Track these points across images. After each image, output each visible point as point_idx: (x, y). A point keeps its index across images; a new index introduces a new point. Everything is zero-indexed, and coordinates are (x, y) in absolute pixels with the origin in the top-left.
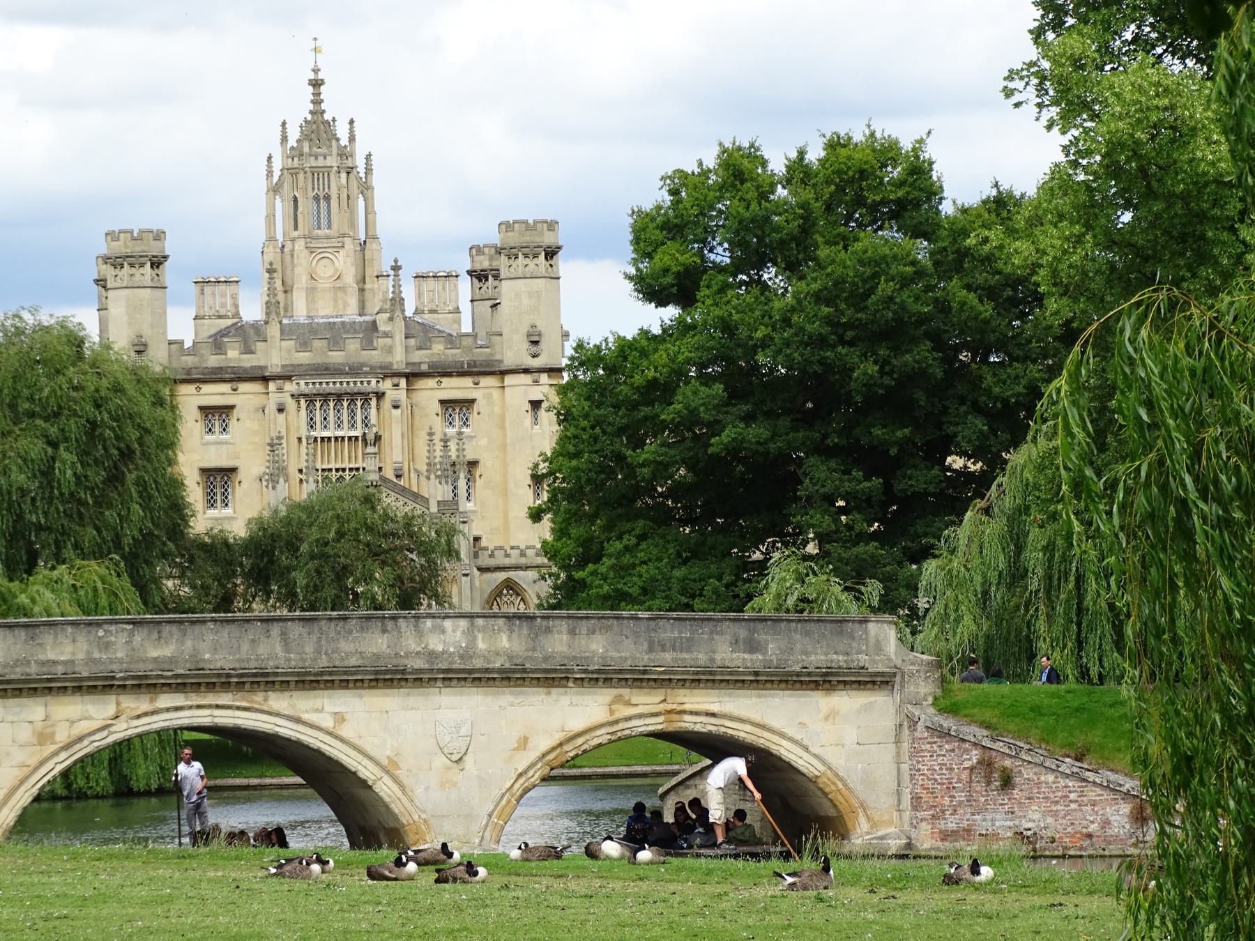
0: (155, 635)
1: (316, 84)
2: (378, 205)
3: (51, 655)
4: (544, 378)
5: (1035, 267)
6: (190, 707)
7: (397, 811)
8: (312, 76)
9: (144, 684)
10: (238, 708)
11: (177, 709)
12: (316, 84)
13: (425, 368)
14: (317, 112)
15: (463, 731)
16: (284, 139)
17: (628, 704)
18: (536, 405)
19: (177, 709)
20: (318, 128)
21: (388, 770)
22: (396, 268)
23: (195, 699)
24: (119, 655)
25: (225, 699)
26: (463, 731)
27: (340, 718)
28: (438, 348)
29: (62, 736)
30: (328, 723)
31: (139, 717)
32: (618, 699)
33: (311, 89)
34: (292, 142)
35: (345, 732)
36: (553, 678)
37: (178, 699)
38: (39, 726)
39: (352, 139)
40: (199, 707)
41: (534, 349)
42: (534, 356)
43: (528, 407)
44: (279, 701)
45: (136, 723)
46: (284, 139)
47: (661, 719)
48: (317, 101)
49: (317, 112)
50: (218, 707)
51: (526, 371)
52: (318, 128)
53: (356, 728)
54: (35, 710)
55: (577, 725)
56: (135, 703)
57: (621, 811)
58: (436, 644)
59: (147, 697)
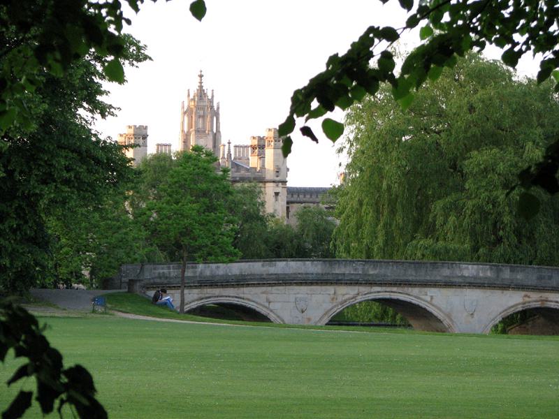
0: (372, 266)
1: (201, 76)
2: (221, 121)
3: (337, 272)
4: (280, 184)
5: (530, 167)
6: (383, 292)
7: (196, 306)
8: (200, 74)
9: (370, 283)
10: (400, 293)
11: (379, 292)
12: (201, 76)
13: (238, 179)
14: (201, 87)
15: (474, 304)
16: (189, 95)
17: (529, 297)
18: (277, 194)
19: (379, 292)
20: (201, 93)
21: (449, 316)
22: (229, 143)
23: (384, 289)
24: (360, 272)
25: (395, 289)
26: (474, 304)
27: (432, 298)
28: (243, 172)
29: (340, 299)
30: (429, 299)
31: (366, 294)
32: (526, 296)
33: (199, 78)
34: (191, 97)
35: (434, 302)
36: (504, 287)
37: (378, 289)
38: (332, 296)
39: (213, 96)
40: (386, 292)
41: (277, 174)
42: (277, 176)
43: (274, 194)
44: (416, 291)
45: (364, 296)
46: (189, 95)
47: (540, 303)
48: (201, 83)
49: (201, 87)
50: (392, 292)
51: (274, 182)
52: (201, 93)
53: (434, 299)
54: (331, 289)
55: (511, 303)
56: (363, 289)
57: (187, 304)
58: (466, 273)
59: (369, 288)
